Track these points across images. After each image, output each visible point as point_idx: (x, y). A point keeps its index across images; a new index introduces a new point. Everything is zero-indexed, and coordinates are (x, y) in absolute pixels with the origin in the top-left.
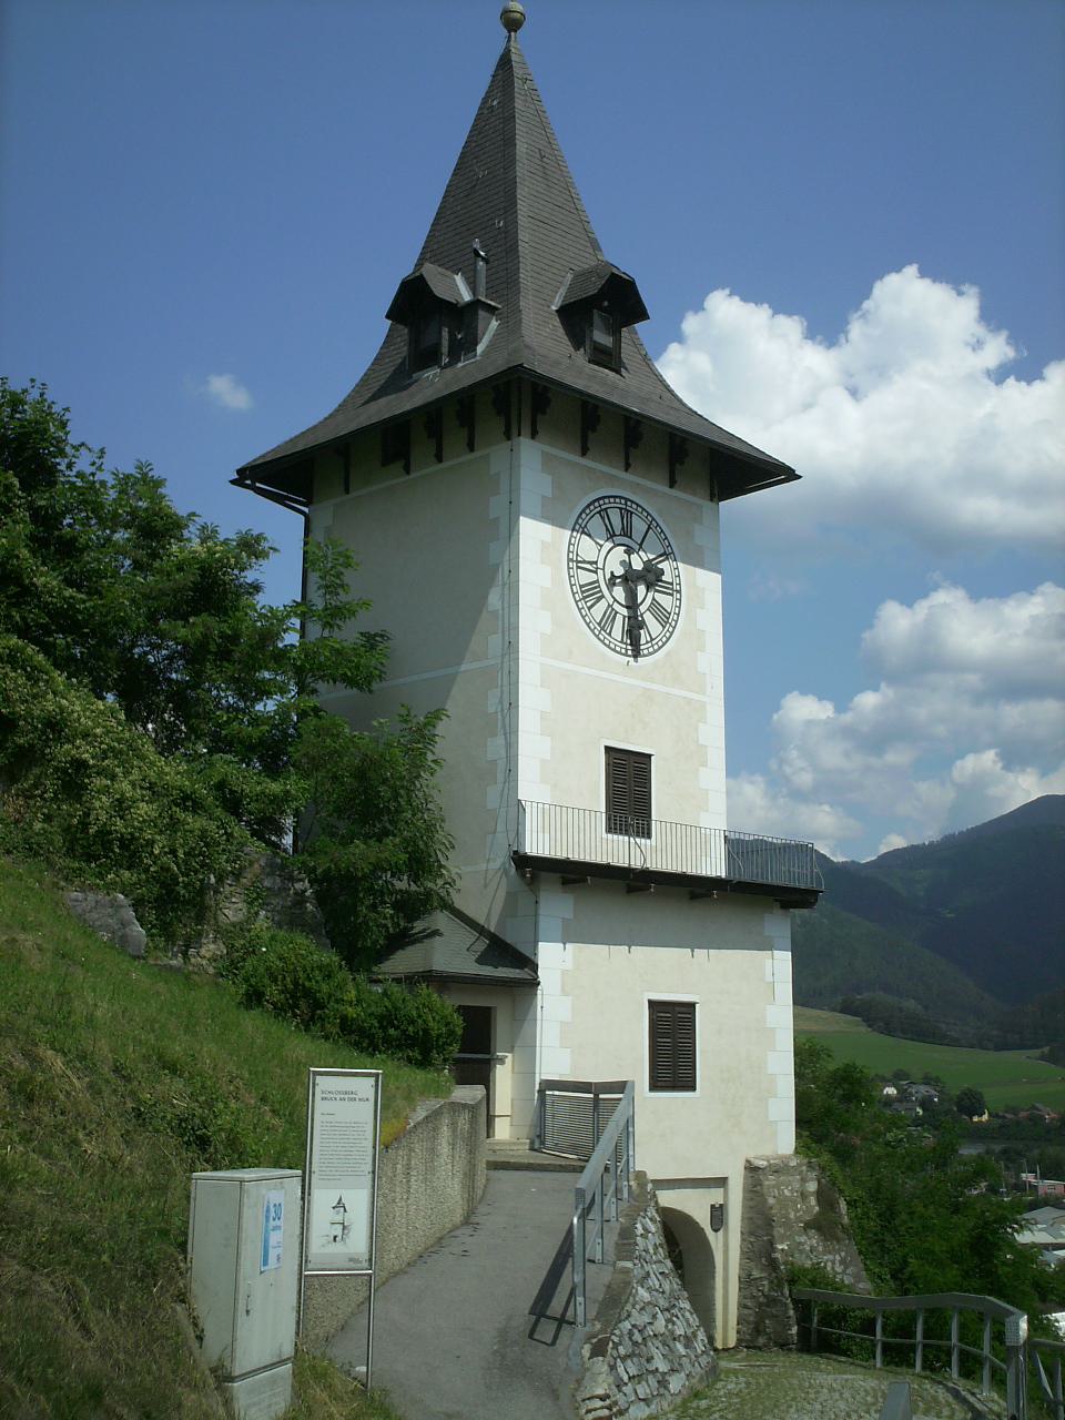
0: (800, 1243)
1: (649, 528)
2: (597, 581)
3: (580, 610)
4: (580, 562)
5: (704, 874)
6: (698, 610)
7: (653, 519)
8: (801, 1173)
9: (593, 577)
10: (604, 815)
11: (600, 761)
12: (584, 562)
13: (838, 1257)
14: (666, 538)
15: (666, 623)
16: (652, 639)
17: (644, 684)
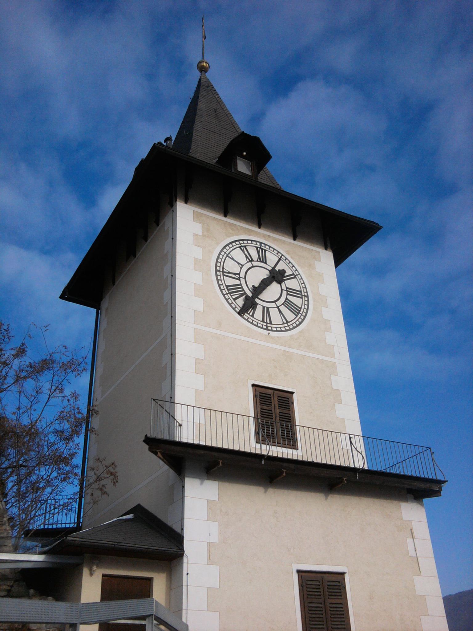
1: (280, 260)
6: (323, 309)
10: (252, 420)
11: (143, 442)
12: (229, 273)
14: (293, 266)
15: (298, 313)
17: (283, 348)
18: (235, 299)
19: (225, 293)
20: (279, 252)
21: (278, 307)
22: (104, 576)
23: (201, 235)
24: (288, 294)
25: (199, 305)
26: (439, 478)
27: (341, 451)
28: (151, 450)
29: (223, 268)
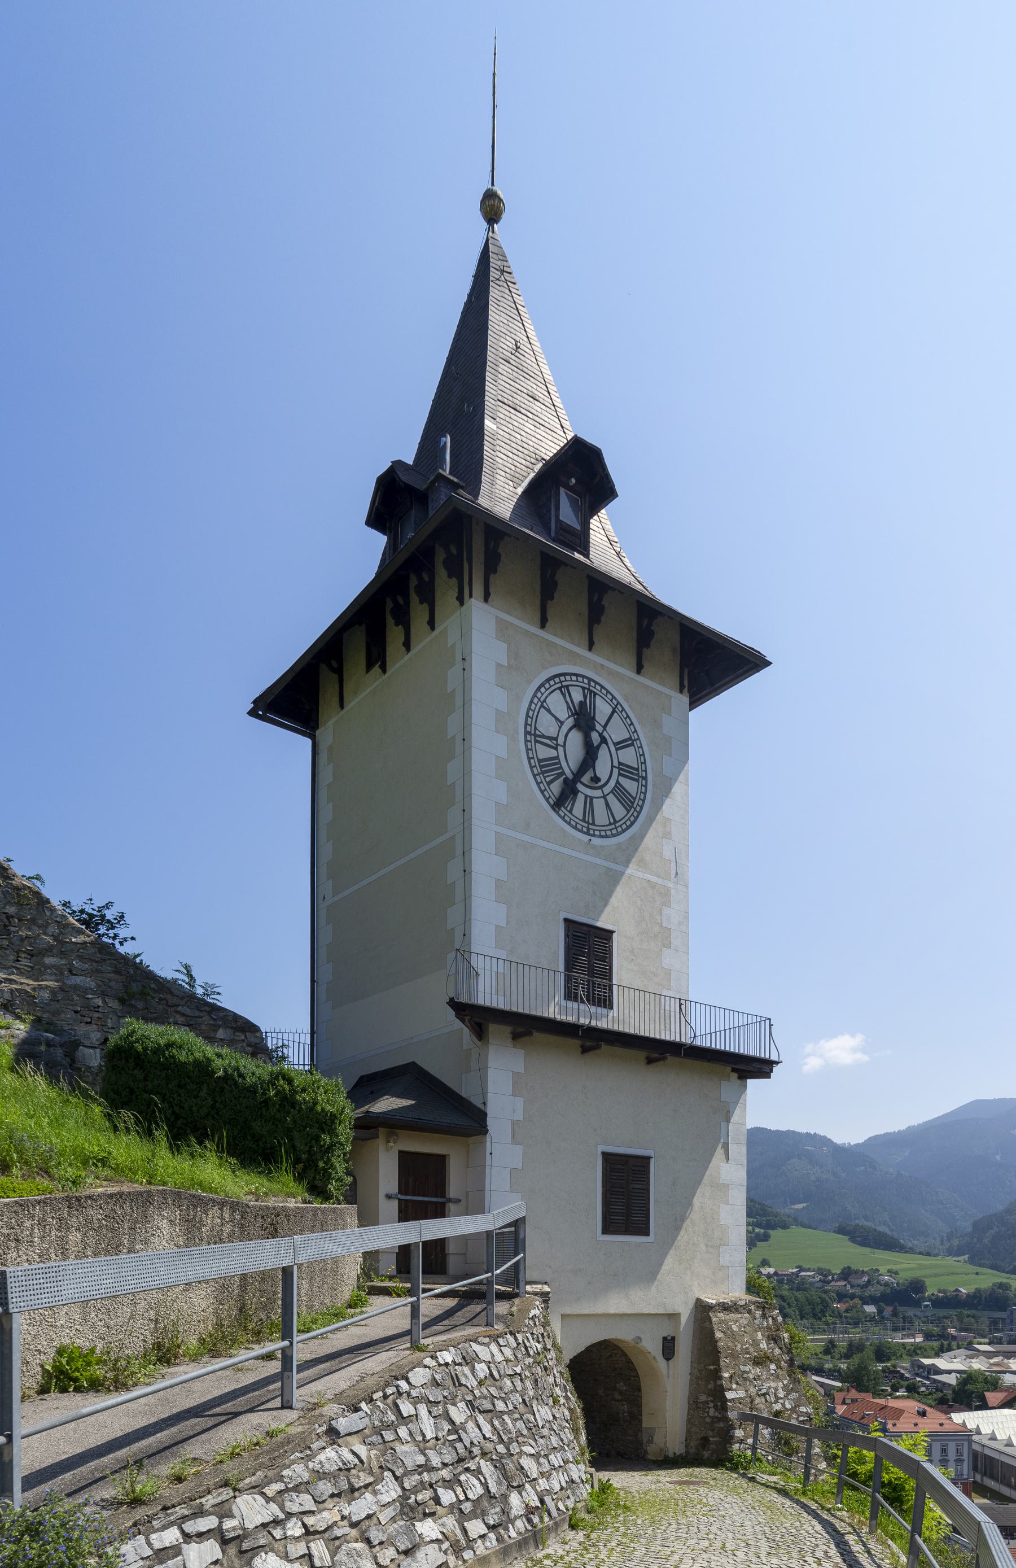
0: (745, 1372)
1: (614, 711)
2: (557, 757)
3: (538, 784)
4: (539, 736)
5: (657, 1037)
7: (618, 703)
8: (749, 1312)
9: (553, 753)
10: (563, 974)
12: (543, 736)
13: (781, 1384)
15: (631, 807)
16: (615, 822)
18: (549, 783)
19: (536, 773)
20: (613, 697)
21: (604, 797)
22: (400, 1152)
23: (506, 664)
24: (620, 774)
25: (501, 792)
26: (772, 1058)
27: (662, 1012)
28: (458, 1016)
29: (536, 728)
